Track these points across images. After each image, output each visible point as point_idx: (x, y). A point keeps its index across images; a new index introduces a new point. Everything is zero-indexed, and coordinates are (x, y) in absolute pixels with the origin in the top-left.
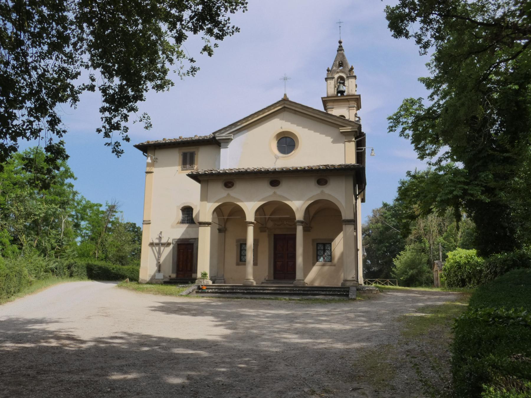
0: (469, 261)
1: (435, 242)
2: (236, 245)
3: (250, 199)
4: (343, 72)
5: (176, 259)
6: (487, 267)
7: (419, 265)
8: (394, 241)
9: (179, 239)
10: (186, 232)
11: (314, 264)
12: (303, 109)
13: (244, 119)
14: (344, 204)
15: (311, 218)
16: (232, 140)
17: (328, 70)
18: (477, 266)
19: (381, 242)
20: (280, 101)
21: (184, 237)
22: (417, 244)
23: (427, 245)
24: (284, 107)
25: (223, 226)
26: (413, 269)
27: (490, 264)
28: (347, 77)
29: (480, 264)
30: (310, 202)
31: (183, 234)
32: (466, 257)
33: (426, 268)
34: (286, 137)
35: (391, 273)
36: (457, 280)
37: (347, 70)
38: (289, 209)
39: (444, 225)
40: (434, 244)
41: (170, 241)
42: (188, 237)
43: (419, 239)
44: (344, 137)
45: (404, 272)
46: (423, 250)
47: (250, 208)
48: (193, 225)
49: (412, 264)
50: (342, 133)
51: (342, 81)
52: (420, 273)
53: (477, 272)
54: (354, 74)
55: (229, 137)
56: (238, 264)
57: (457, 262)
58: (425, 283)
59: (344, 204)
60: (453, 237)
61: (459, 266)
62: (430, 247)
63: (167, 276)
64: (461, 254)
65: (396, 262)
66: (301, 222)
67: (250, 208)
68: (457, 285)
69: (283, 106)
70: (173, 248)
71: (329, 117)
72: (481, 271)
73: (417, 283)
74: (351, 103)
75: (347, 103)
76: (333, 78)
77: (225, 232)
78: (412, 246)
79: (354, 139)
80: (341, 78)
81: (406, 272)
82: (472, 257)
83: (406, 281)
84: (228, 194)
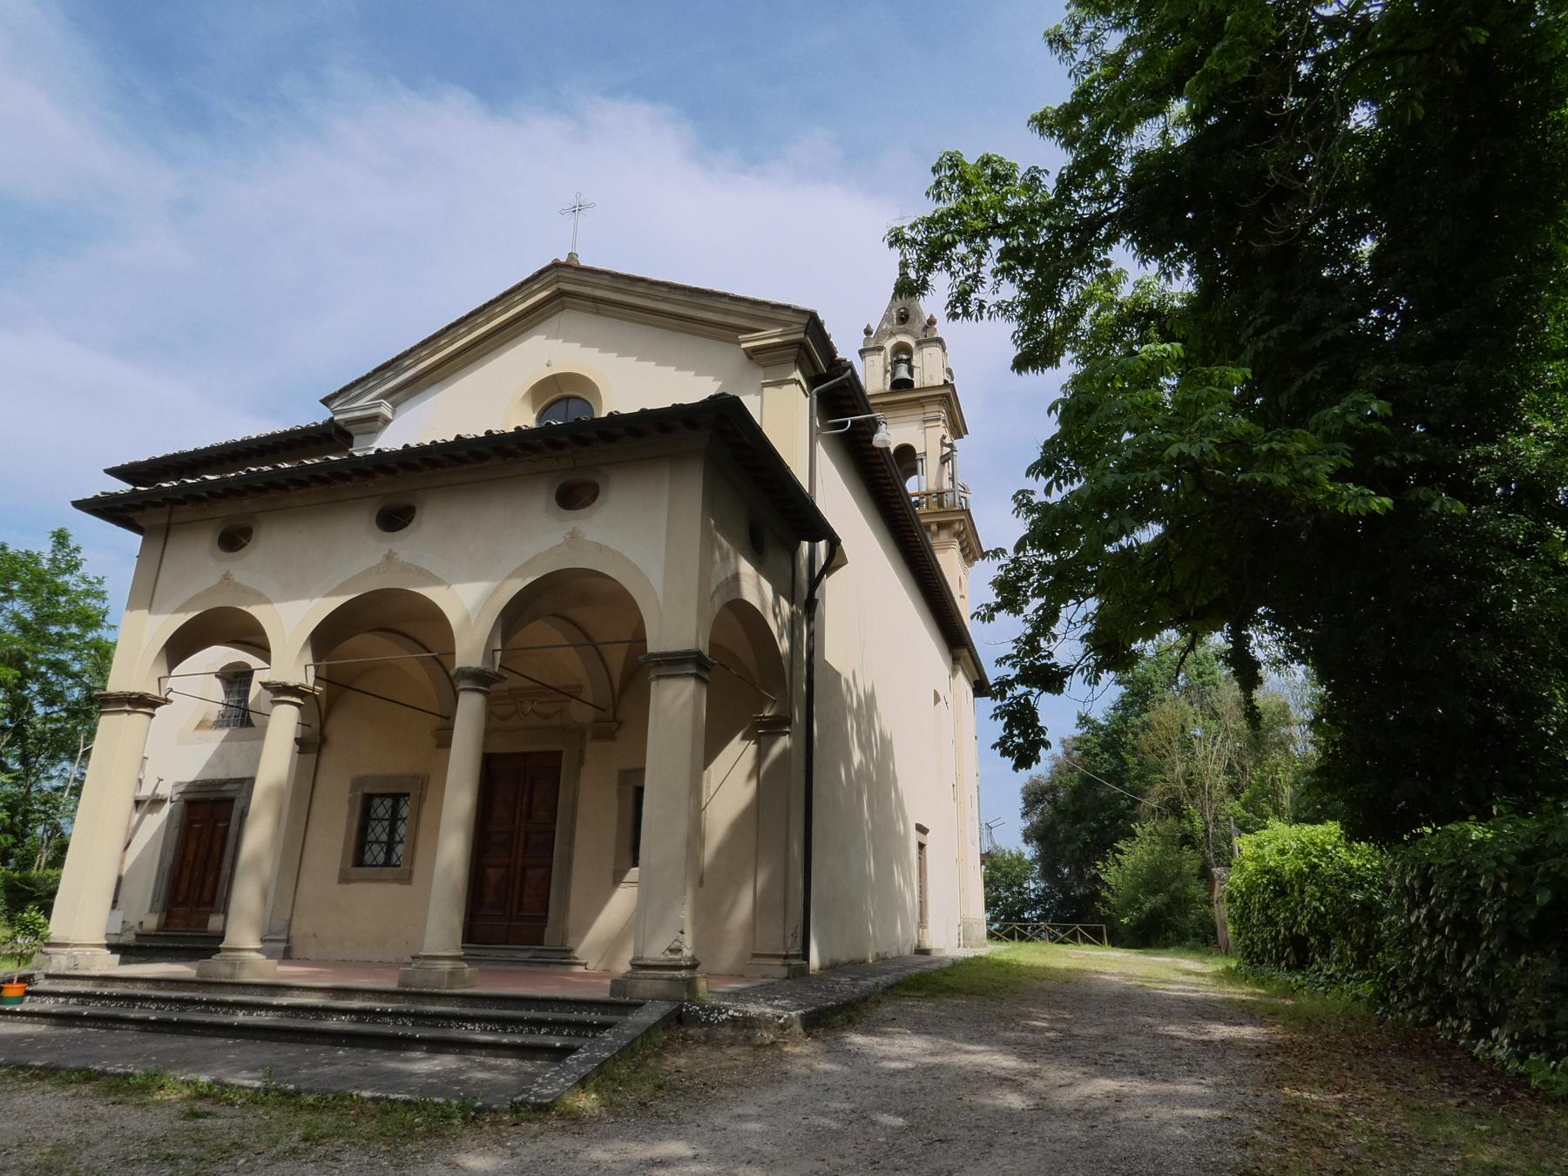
0: (1314, 867)
1: (1221, 818)
2: (351, 801)
3: (295, 590)
4: (906, 332)
5: (170, 858)
6: (1406, 891)
7: (1173, 880)
8: (1110, 817)
9: (194, 783)
10: (220, 755)
11: (617, 879)
12: (618, 290)
13: (424, 344)
14: (657, 583)
15: (617, 683)
16: (387, 421)
17: (868, 332)
18: (1351, 887)
19: (1078, 817)
20: (541, 272)
21: (210, 776)
22: (1170, 821)
23: (1198, 823)
24: (560, 294)
25: (316, 726)
26: (1155, 892)
27: (1427, 882)
28: (919, 343)
29: (1363, 879)
30: (518, 585)
31: (209, 765)
32: (1303, 852)
33: (1196, 889)
34: (568, 398)
35: (1098, 905)
36: (1275, 939)
37: (918, 327)
38: (435, 616)
39: (1243, 768)
40: (1216, 819)
41: (166, 790)
42: (220, 774)
43: (1174, 808)
44: (761, 372)
45: (1133, 902)
46: (1187, 839)
47: (468, 603)
48: (246, 731)
49: (1154, 880)
50: (752, 354)
51: (902, 354)
52: (1180, 903)
53: (1353, 912)
54: (939, 334)
55: (374, 411)
56: (344, 879)
57: (1269, 871)
58: (1196, 935)
59: (657, 583)
60: (1270, 801)
61: (1278, 886)
62: (1206, 831)
63: (134, 922)
64: (1280, 841)
65: (1110, 875)
66: (480, 679)
67: (468, 603)
68: (1279, 959)
69: (553, 288)
70: (171, 811)
71: (704, 301)
72: (1370, 910)
73: (1170, 934)
74: (928, 409)
75: (920, 411)
76: (881, 349)
77: (319, 751)
78: (1148, 827)
79: (797, 375)
80: (902, 348)
81: (1136, 900)
82: (1325, 852)
83: (1138, 928)
84: (226, 577)
